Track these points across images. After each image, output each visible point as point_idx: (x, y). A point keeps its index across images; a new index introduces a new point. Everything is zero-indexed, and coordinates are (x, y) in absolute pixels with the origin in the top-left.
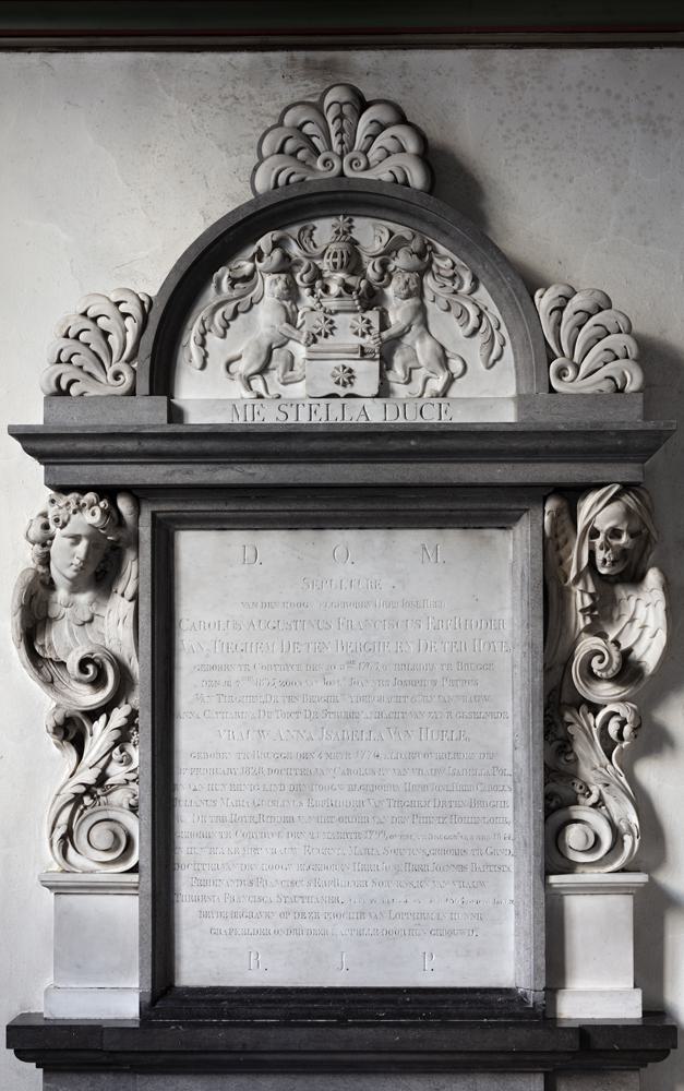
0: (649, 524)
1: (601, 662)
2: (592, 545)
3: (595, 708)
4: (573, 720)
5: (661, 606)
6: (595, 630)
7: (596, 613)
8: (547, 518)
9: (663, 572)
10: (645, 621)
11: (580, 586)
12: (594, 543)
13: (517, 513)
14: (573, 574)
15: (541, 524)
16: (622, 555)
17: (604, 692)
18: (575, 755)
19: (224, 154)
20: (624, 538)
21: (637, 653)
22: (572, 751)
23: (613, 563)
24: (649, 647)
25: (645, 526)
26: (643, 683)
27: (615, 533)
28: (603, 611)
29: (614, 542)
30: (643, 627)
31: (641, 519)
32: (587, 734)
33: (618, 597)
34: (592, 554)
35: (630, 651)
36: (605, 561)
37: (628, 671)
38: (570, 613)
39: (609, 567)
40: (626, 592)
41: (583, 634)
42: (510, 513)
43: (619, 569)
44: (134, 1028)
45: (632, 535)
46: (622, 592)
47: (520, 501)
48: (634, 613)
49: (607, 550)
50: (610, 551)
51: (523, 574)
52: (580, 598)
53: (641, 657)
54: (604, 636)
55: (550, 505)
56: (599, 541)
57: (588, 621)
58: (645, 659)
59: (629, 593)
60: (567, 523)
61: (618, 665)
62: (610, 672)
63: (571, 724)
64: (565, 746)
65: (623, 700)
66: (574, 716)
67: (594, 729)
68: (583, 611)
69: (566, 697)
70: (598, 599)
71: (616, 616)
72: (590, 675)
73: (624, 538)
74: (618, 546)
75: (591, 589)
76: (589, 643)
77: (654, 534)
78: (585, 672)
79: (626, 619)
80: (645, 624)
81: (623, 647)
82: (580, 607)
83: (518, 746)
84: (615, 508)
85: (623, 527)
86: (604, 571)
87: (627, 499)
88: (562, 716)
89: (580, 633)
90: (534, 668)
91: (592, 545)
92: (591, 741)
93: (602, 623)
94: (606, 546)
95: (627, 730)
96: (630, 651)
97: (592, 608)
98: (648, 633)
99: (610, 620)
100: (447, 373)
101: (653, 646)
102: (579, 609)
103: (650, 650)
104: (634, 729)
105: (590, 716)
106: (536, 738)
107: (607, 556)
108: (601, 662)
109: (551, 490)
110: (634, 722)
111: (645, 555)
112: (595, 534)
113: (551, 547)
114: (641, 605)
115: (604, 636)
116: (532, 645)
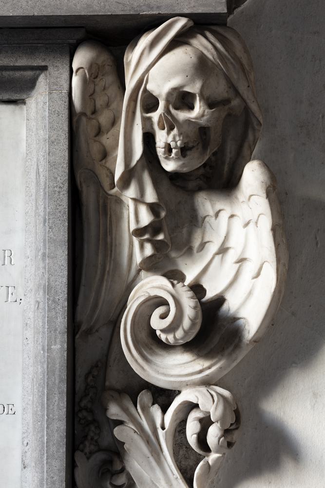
0: (242, 88)
1: (163, 317)
2: (147, 121)
3: (163, 397)
4: (123, 417)
5: (266, 222)
6: (162, 264)
7: (161, 237)
8: (76, 80)
9: (267, 165)
10: (243, 251)
11: (131, 192)
12: (150, 119)
13: (29, 74)
14: (119, 170)
15: (65, 91)
17: (176, 368)
18: (130, 478)
20: (199, 108)
21: (232, 304)
22: (123, 470)
23: (184, 151)
24: (250, 293)
25: (237, 93)
26: (241, 355)
27: (182, 99)
28: (175, 234)
30: (241, 261)
31: (228, 79)
32: (148, 442)
33: (202, 212)
34: (149, 139)
35: (220, 300)
36: (169, 149)
37: (213, 329)
38: (121, 237)
39: (177, 159)
41: (143, 273)
42: (18, 74)
43: (195, 162)
45: (210, 104)
46: (207, 204)
47: (31, 50)
48: (226, 238)
49: (171, 129)
50: (175, 131)
51: (38, 173)
52: (135, 211)
53: (239, 309)
54: (175, 276)
55: (81, 58)
56: (155, 116)
57: (149, 250)
58: (242, 314)
59: (219, 206)
60: (110, 79)
61: (193, 322)
62: (179, 333)
63: (120, 423)
64: (111, 462)
65: (206, 383)
66: (126, 410)
67: (161, 432)
68: (139, 232)
69: (114, 378)
70: (163, 214)
71: (196, 244)
72: (151, 342)
73: (199, 108)
74: (188, 121)
75: (151, 196)
76: (152, 285)
77: (254, 107)
78: (143, 335)
79: (213, 248)
80: (240, 250)
81: (210, 294)
82: (133, 227)
83: (27, 462)
84: (182, 56)
85: (194, 88)
86: (170, 166)
87: (201, 43)
88: (106, 410)
89: (139, 271)
90: (52, 329)
91: (147, 121)
92: (156, 452)
93: (173, 255)
94: (170, 123)
95: (213, 435)
96: (220, 300)
97: (154, 229)
98: (249, 269)
99: (187, 249)
101: (256, 293)
102: (131, 230)
103: (251, 302)
104: (226, 432)
105: (156, 411)
106: (53, 449)
107: (170, 139)
108: (163, 317)
109: (80, 34)
110: (222, 419)
111: (246, 146)
112: (151, 103)
113: (86, 128)
114: (237, 223)
115: (175, 276)
116: (49, 289)
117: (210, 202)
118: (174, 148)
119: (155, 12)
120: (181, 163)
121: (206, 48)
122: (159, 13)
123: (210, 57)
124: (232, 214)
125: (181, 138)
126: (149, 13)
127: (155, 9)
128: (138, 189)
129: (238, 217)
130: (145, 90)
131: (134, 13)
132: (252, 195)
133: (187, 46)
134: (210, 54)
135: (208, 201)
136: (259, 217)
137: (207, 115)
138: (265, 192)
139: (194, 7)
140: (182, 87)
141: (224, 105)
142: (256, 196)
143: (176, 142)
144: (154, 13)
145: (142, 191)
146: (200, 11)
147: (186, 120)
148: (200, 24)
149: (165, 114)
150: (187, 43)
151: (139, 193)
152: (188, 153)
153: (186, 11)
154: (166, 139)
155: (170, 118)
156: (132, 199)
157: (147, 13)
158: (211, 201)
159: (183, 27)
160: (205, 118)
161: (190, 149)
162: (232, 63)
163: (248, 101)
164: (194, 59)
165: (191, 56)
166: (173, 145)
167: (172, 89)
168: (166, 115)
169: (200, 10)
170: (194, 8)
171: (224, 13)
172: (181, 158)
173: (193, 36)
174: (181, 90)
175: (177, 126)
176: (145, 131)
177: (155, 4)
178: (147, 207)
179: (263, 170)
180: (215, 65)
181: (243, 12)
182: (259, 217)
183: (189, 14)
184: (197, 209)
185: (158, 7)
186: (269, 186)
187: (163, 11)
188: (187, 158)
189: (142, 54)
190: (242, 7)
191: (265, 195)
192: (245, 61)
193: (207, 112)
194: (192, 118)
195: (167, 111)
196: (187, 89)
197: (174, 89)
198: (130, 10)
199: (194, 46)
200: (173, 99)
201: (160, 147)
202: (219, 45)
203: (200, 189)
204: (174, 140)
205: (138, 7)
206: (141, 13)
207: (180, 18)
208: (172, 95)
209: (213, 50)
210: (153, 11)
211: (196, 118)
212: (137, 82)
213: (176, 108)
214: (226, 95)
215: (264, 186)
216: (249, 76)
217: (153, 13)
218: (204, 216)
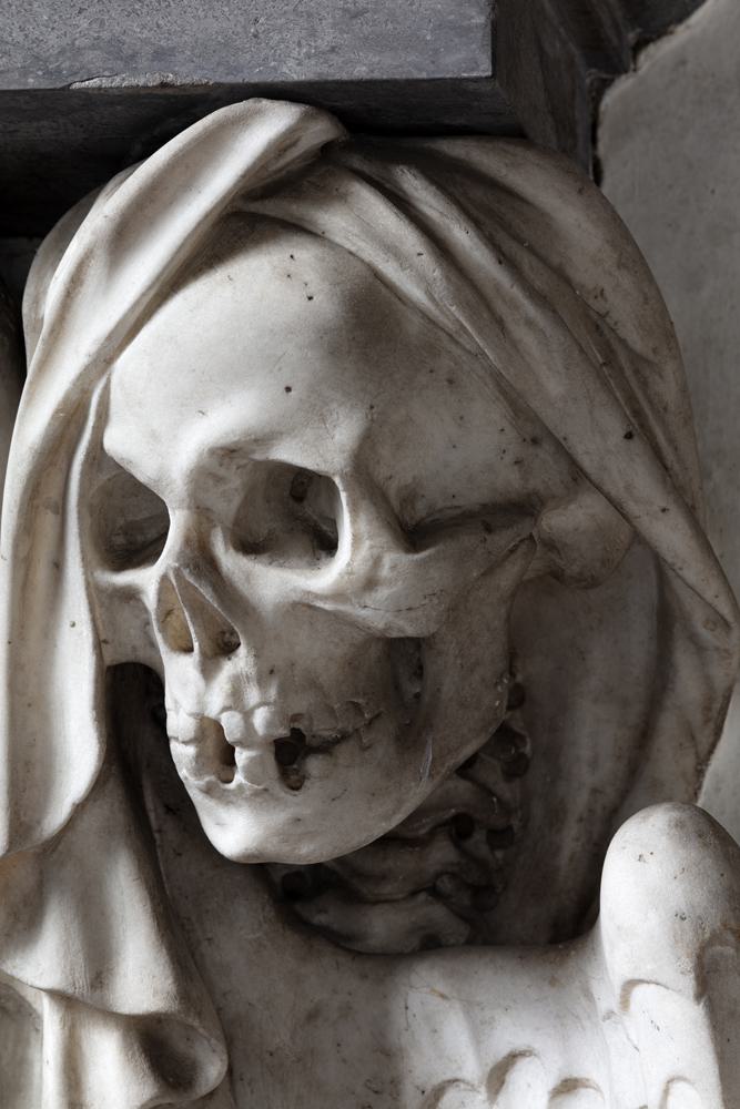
2: (112, 606)
16: (367, 698)
19: (494, 681)
20: (357, 539)
23: (291, 754)
29: (273, 583)
31: (518, 408)
33: (422, 1068)
39: (259, 797)
40: (479, 1031)
44: (486, 78)
49: (223, 647)
50: (241, 662)
59: (508, 1034)
73: (357, 539)
74: (302, 609)
75: (142, 980)
84: (266, 288)
85: (323, 449)
86: (233, 831)
87: (363, 224)
100: (700, 804)
117: (468, 1013)
118: (242, 743)
119: (146, 79)
120: (279, 817)
121: (392, 250)
122: (163, 85)
123: (415, 292)
124: (566, 1075)
125: (273, 693)
126: (117, 82)
127: (143, 63)
128: (77, 945)
129: (598, 1089)
130: (98, 455)
131: (45, 85)
132: (641, 981)
133: (298, 239)
134: (414, 276)
135: (457, 1005)
136: (666, 1092)
137: (390, 582)
138: (688, 964)
139: (333, 50)
140: (263, 439)
141: (489, 529)
142: (653, 986)
143: (247, 715)
144: (141, 81)
145: (98, 959)
146: (360, 71)
147: (295, 605)
148: (372, 130)
149: (186, 573)
150: (298, 228)
151: (80, 959)
152: (314, 765)
153: (294, 71)
154: (201, 702)
155: (207, 593)
156: (55, 995)
157: (105, 83)
158: (469, 1007)
159: (280, 146)
160: (382, 593)
161: (326, 748)
162: (529, 323)
163: (633, 508)
164: (326, 306)
165: (312, 290)
166: (231, 724)
167: (213, 452)
168: (191, 580)
169: (362, 66)
170: (332, 56)
171: (476, 80)
172: (278, 789)
173: (327, 194)
174: (258, 456)
175: (245, 632)
176: (108, 661)
177: (146, 41)
178: (125, 1036)
179: (693, 853)
180: (435, 338)
181: (683, 62)
182: (666, 1092)
183: (310, 84)
184: (401, 1049)
185: (160, 55)
186: (715, 938)
187: (186, 74)
188: (313, 789)
189: (76, 281)
190: (682, 35)
191: (688, 983)
192: (623, 310)
193: (393, 568)
194: (317, 596)
195: (201, 560)
196: (290, 453)
197: (227, 454)
198: (25, 72)
199: (338, 240)
200: (227, 505)
201: (177, 739)
202: (462, 236)
203: (430, 945)
204: (236, 699)
205: (62, 52)
206: (76, 86)
207: (265, 103)
208: (219, 480)
209: (427, 263)
210: (135, 72)
211: (338, 595)
212: (54, 417)
213: (249, 546)
214: (509, 480)
215: (689, 936)
216: (644, 384)
217: (134, 81)
218: (436, 1081)
